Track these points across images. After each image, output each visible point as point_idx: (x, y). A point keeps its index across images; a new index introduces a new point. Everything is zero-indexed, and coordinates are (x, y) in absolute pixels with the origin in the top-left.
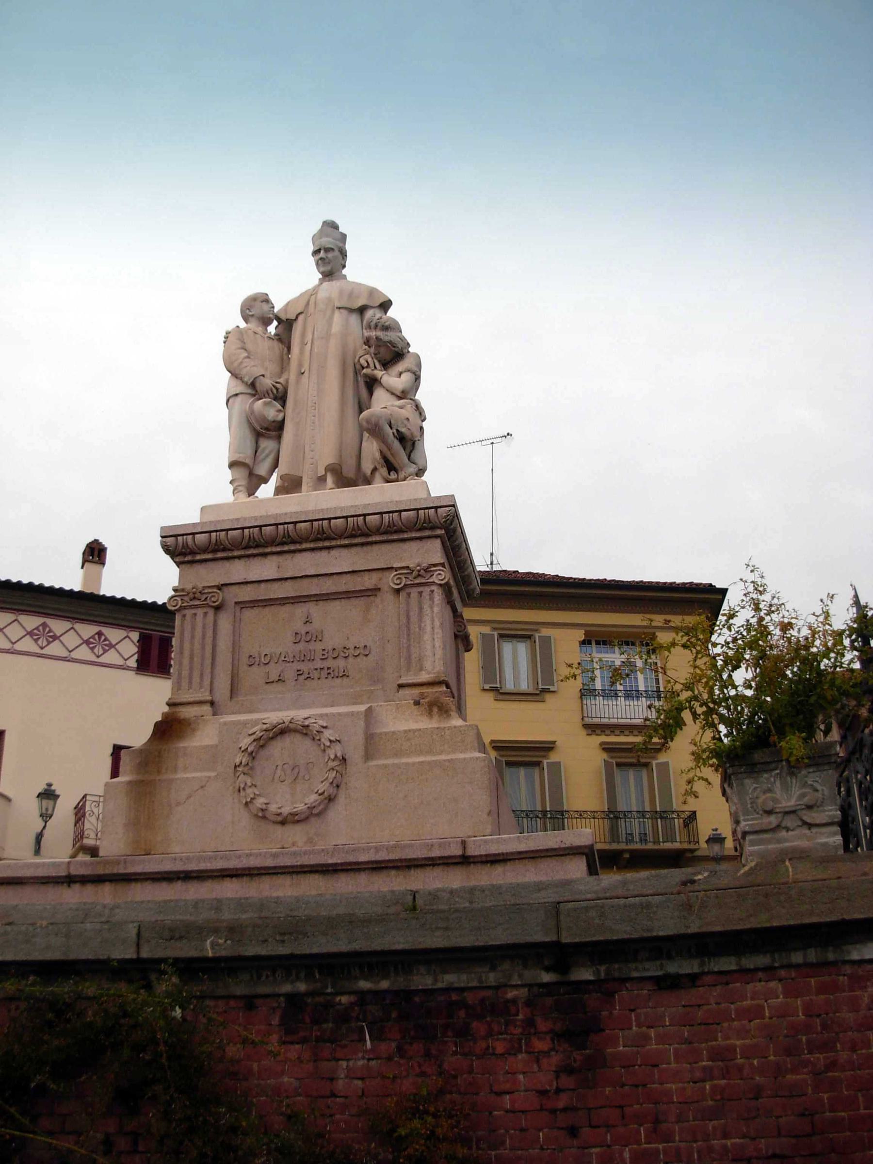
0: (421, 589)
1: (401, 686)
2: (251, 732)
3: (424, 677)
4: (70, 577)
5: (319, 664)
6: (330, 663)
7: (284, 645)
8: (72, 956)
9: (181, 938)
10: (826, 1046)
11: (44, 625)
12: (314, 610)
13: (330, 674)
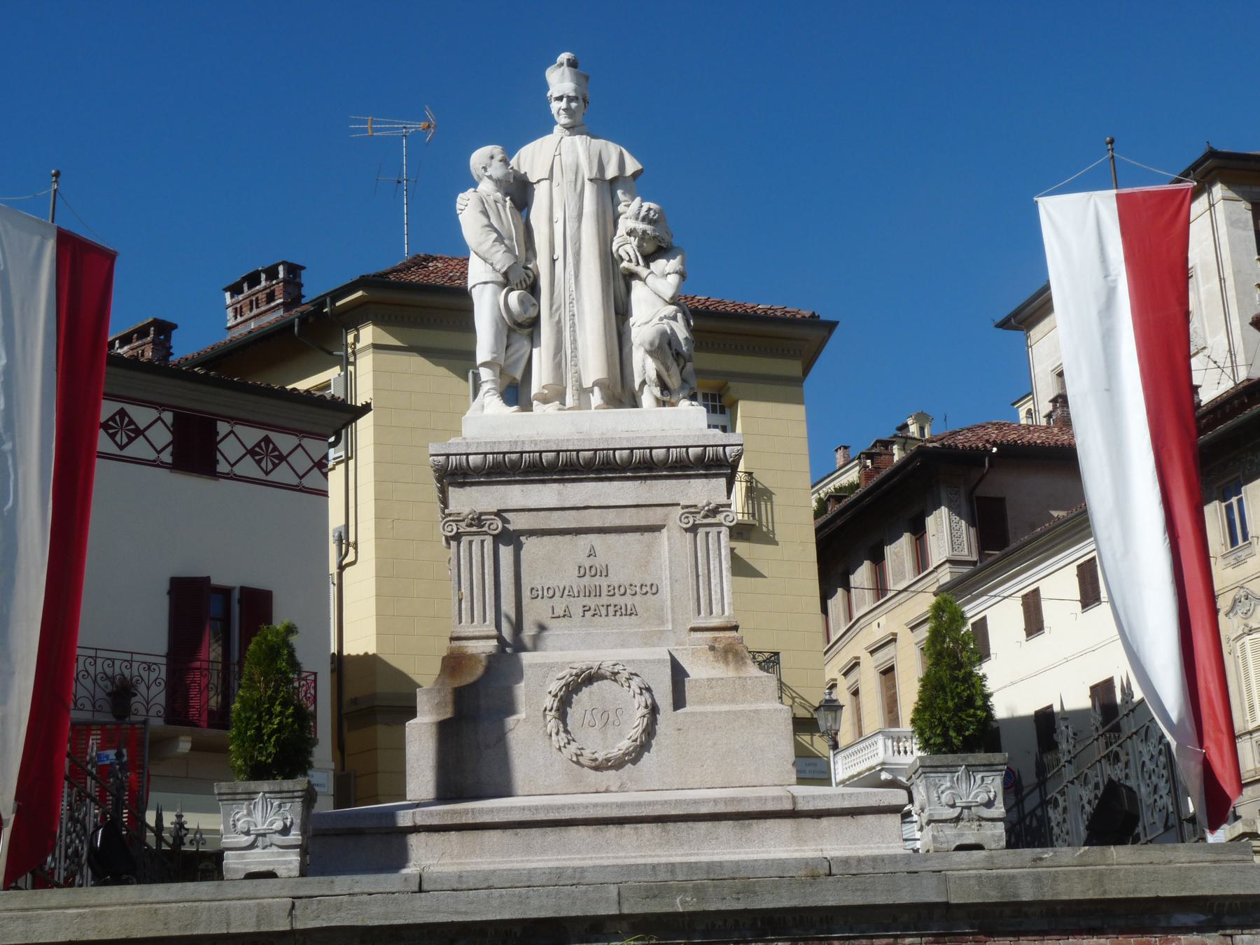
0: (708, 529)
1: (694, 630)
2: (560, 675)
3: (715, 622)
4: (983, 823)
5: (605, 600)
6: (618, 600)
7: (569, 578)
8: (563, 914)
9: (655, 897)
11: (267, 440)
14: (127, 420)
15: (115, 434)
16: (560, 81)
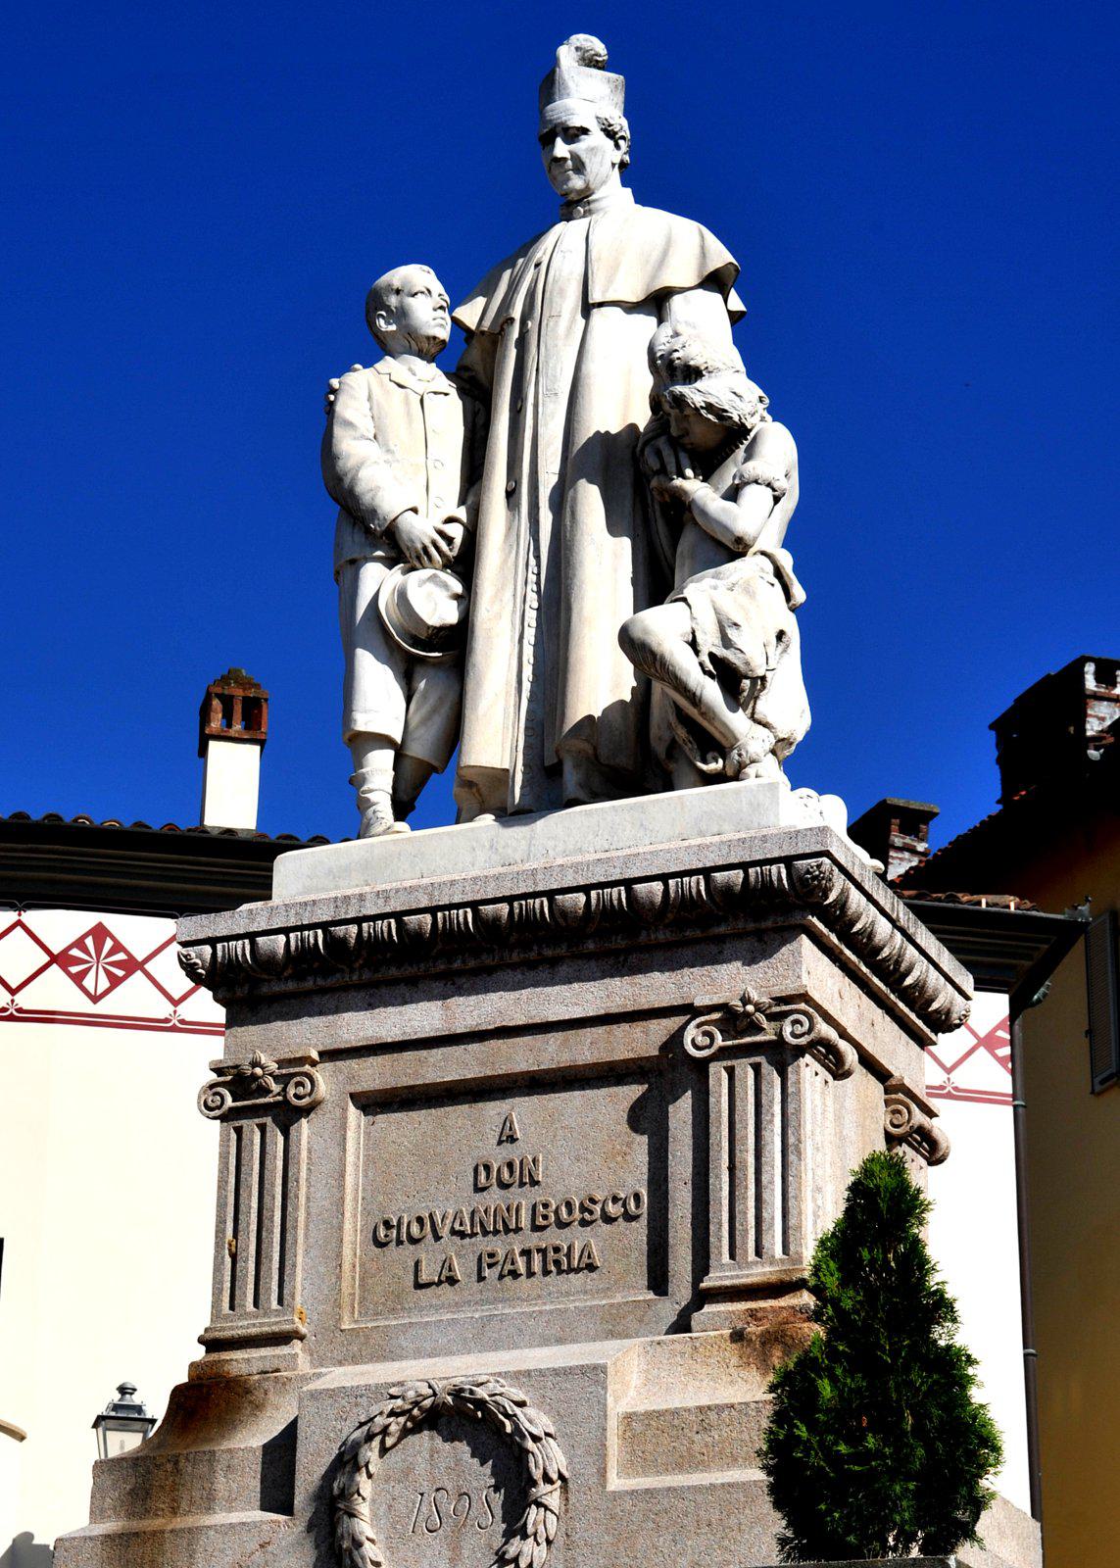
3: (757, 1273)
6: (552, 1237)
11: (100, 933)
12: (522, 1110)
13: (559, 1264)
15: (84, 974)
16: (589, 95)
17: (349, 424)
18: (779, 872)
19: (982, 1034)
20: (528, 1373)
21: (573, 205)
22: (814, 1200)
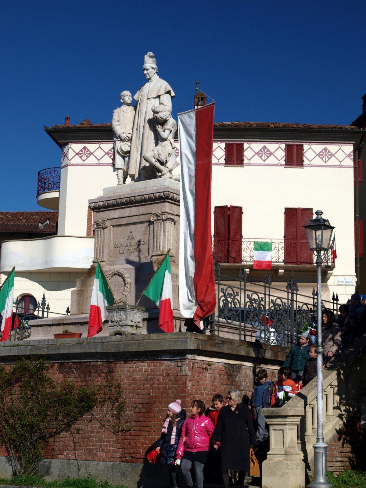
3: (159, 253)
10: (153, 379)
14: (327, 151)
16: (150, 63)
17: (114, 119)
18: (162, 194)
19: (348, 154)
20: (126, 269)
21: (148, 80)
22: (168, 241)
